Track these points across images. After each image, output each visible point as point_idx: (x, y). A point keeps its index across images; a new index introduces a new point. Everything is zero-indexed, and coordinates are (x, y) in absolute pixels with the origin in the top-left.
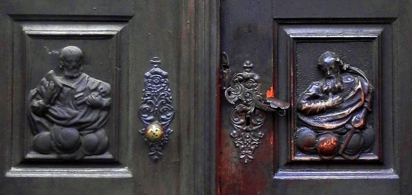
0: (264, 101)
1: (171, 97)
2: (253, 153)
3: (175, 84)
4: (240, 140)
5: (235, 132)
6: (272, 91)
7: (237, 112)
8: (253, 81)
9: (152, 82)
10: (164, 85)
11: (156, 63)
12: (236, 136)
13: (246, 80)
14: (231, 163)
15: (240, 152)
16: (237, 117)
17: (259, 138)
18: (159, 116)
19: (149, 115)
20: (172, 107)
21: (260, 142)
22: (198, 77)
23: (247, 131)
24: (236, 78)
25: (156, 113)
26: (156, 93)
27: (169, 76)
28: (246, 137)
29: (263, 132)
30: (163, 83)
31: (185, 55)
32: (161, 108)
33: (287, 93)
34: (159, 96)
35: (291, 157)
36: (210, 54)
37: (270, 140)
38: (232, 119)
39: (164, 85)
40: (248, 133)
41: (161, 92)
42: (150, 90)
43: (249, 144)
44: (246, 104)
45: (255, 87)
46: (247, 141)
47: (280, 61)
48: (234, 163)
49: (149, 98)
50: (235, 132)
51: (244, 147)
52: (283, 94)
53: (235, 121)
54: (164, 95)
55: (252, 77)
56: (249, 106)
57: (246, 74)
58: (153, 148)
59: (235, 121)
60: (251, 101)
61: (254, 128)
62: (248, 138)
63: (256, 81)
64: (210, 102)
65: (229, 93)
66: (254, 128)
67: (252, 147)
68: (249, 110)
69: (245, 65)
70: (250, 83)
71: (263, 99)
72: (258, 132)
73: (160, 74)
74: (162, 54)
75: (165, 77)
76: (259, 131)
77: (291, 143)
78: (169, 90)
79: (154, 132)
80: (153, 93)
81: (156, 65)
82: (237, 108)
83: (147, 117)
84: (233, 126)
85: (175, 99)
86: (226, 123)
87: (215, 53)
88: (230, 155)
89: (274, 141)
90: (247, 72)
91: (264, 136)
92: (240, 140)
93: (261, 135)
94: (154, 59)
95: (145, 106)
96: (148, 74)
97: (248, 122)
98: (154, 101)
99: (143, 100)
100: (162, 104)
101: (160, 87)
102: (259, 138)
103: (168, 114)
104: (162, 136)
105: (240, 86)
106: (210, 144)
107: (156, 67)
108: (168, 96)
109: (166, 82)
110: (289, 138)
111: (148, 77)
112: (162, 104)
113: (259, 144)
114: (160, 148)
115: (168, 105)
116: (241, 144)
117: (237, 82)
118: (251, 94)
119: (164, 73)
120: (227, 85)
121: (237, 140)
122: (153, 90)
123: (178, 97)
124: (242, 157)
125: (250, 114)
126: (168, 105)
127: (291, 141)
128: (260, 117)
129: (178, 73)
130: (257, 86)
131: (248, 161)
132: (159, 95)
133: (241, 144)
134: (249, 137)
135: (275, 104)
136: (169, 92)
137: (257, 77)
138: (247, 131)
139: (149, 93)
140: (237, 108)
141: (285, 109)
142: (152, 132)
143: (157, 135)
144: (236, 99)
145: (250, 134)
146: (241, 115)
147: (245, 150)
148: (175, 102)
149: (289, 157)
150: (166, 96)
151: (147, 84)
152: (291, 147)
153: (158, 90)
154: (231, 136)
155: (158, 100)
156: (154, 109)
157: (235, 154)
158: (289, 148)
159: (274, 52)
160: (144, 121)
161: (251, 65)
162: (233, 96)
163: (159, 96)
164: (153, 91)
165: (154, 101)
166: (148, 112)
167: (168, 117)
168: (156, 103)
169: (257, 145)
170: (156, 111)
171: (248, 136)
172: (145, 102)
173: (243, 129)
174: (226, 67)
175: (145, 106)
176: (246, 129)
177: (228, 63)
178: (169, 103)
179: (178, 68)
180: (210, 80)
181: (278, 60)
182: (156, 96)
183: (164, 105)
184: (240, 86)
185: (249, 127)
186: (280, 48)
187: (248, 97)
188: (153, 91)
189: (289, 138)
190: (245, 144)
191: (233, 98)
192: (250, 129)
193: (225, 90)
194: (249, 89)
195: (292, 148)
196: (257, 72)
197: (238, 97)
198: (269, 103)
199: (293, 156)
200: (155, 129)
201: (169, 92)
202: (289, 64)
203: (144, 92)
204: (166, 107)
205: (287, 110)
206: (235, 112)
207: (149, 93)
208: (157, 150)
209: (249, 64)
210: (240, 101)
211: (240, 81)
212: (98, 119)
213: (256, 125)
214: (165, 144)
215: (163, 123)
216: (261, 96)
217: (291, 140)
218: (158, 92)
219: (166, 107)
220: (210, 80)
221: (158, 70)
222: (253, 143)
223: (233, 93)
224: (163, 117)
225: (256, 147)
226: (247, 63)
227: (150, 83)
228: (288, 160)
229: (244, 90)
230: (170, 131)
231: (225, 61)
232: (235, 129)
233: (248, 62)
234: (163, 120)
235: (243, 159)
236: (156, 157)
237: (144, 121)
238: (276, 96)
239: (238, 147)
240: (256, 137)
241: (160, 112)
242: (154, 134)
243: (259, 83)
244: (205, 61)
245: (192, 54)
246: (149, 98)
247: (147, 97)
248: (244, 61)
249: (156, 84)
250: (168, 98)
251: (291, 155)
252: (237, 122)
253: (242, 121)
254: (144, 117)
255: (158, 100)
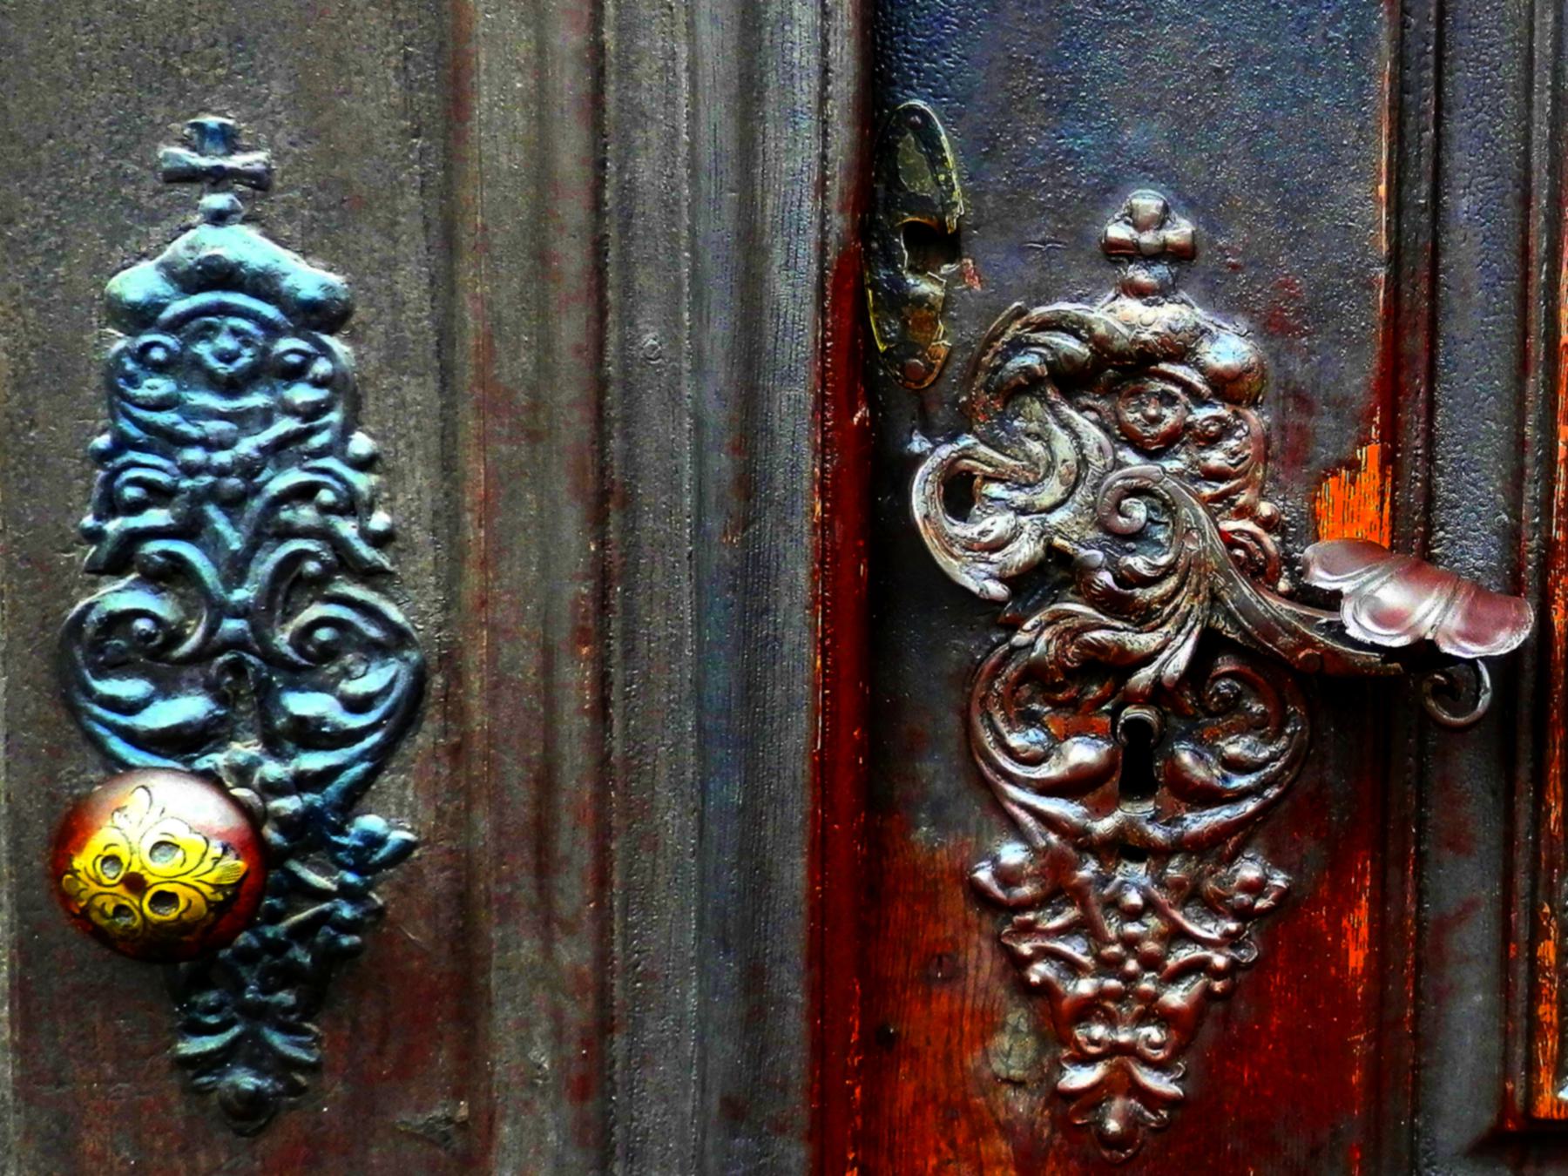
0: (1296, 577)
1: (380, 521)
2: (1178, 1052)
3: (419, 392)
4: (1065, 931)
5: (1012, 854)
6: (1370, 478)
7: (1035, 674)
8: (1187, 387)
9: (180, 366)
10: (302, 394)
11: (218, 179)
12: (1026, 890)
13: (1116, 371)
14: (980, 1132)
15: (1067, 1040)
16: (1031, 719)
17: (1243, 914)
18: (266, 699)
19: (166, 688)
20: (395, 614)
21: (1248, 955)
22: (628, 321)
23: (1126, 846)
24: (1018, 346)
25: (237, 668)
26: (222, 472)
27: (361, 312)
28: (1113, 903)
29: (1276, 858)
30: (295, 374)
31: (498, 96)
32: (288, 616)
33: (1515, 507)
34: (257, 504)
35: (1532, 1091)
36: (749, 92)
37: (1339, 934)
38: (988, 739)
39: (302, 394)
40: (1138, 872)
41: (281, 467)
42: (170, 441)
43: (1151, 963)
44: (1115, 605)
45: (1212, 441)
46: (1130, 943)
47: (1462, 205)
48: (1007, 1130)
49: (157, 517)
50: (1012, 854)
51: (1102, 994)
52: (1472, 539)
53: (1011, 752)
54: (305, 493)
55: (1180, 348)
56: (1144, 618)
57: (1125, 317)
58: (212, 997)
59: (1011, 752)
60: (1169, 569)
61: (1199, 822)
62: (1134, 914)
63: (1225, 386)
64: (752, 576)
65: (959, 493)
66: (1199, 822)
67: (1176, 997)
68: (1148, 659)
69: (1118, 231)
70: (1168, 399)
71: (1290, 562)
72: (1230, 860)
73: (262, 284)
74: (277, 89)
75: (317, 317)
76: (1237, 853)
77: (1533, 960)
78: (361, 444)
79: (138, 860)
80: (190, 470)
81: (218, 201)
82: (1037, 638)
83: (133, 708)
84: (996, 802)
85: (419, 535)
86: (935, 772)
87: (805, 91)
88: (972, 1061)
89: (1381, 932)
90: (1138, 292)
91: (1284, 896)
92: (1065, 931)
93: (1256, 888)
94: (203, 137)
95: (119, 596)
96: (138, 282)
97: (1136, 768)
98: (212, 546)
99: (95, 536)
100: (291, 584)
101: (266, 417)
102: (1243, 914)
103: (347, 674)
104: (233, 906)
105: (1066, 425)
106: (755, 977)
107: (218, 218)
108: (351, 505)
109: (322, 367)
110: (1519, 918)
111: (141, 316)
112: (291, 584)
113: (1234, 965)
114: (286, 997)
115: (357, 592)
116: (1073, 968)
117: (1031, 384)
118: (1166, 507)
119: (308, 278)
120: (941, 415)
121: (1028, 929)
122: (190, 442)
123: (447, 519)
124: (1079, 1078)
125: (1159, 693)
126: (357, 592)
127: (1532, 946)
128: (1250, 726)
129: (444, 286)
130: (1226, 430)
131: (1131, 1121)
132: (258, 491)
133: (1073, 968)
134: (1150, 905)
135: (1387, 609)
136: (364, 464)
137: (1229, 349)
138: (1126, 846)
139: (153, 467)
140: (1037, 638)
141: (1485, 659)
142: (113, 860)
143: (164, 899)
144: (1024, 551)
145: (1160, 882)
146: (1073, 705)
147: (1111, 1021)
148: (422, 564)
149: (1517, 1088)
150: (325, 509)
151: (133, 381)
152: (1534, 996)
153: (247, 446)
154: (978, 893)
155: (255, 543)
156: (212, 630)
157: (1011, 1051)
158: (1520, 1008)
159: (1399, 111)
160: (118, 746)
161: (1180, 231)
162: (999, 524)
163: (257, 504)
164: (194, 455)
165: (212, 546)
166: (158, 658)
167: (357, 705)
168: (236, 570)
169: (1217, 974)
170: (227, 646)
171: (1134, 898)
172: (122, 559)
173: (1086, 832)
174: (935, 243)
175: (119, 596)
176: (1120, 831)
177: (949, 207)
178: (370, 575)
179: (447, 239)
180: (750, 354)
181: (1436, 194)
182: (233, 504)
183: (317, 587)
184: (1066, 425)
185: (1148, 807)
186: (1462, 77)
187: (1139, 536)
188: (194, 455)
189: (1519, 918)
190: (1109, 966)
191: (979, 548)
192: (1157, 833)
193: (920, 459)
194: (1151, 456)
195: (1547, 1012)
196: (1225, 299)
197: (1045, 534)
198: (1332, 600)
199: (1545, 1078)
200: (165, 831)
201: (364, 464)
202: (1538, 222)
203: (102, 457)
204: (333, 611)
205: (1504, 666)
206: (1011, 671)
207: (153, 467)
208: (258, 1014)
209: (1161, 222)
210: (1054, 572)
211: (1070, 380)
212: (392, 682)
213: (1209, 797)
214: (331, 957)
215: (314, 761)
216: (1268, 524)
217: (1537, 933)
218: (248, 469)
219: (333, 611)
220: (750, 354)
221: (243, 245)
222: (1185, 954)
223: (995, 490)
224: (303, 704)
225: (1207, 992)
226: (1142, 211)
227: (160, 368)
228: (1505, 1098)
229: (1097, 463)
230: (373, 841)
231: (923, 186)
232: (1016, 830)
233: (1148, 201)
234: (309, 734)
235: (1092, 1097)
236: (247, 1081)
237: (118, 746)
238: (1412, 544)
239: (1046, 987)
240: (1213, 907)
241: (273, 659)
242: (135, 883)
243: (1254, 404)
244: (693, 164)
245: (569, 82)
246: (157, 517)
247: (136, 508)
248: (1108, 190)
249: (231, 387)
250: (346, 528)
251: (1531, 1066)
252: (1035, 761)
253: (1083, 753)
254: (113, 703)
255: (255, 543)
